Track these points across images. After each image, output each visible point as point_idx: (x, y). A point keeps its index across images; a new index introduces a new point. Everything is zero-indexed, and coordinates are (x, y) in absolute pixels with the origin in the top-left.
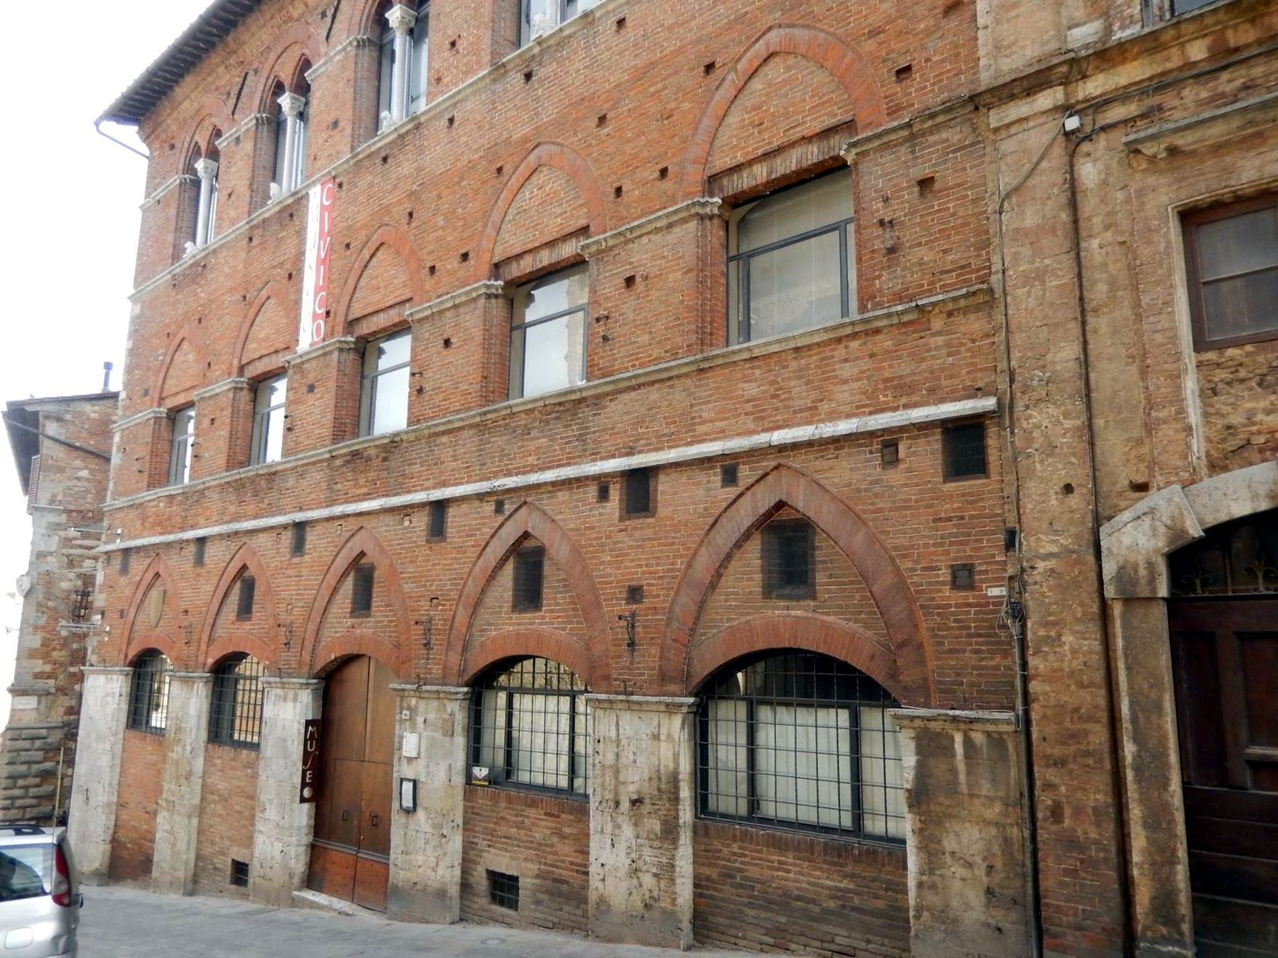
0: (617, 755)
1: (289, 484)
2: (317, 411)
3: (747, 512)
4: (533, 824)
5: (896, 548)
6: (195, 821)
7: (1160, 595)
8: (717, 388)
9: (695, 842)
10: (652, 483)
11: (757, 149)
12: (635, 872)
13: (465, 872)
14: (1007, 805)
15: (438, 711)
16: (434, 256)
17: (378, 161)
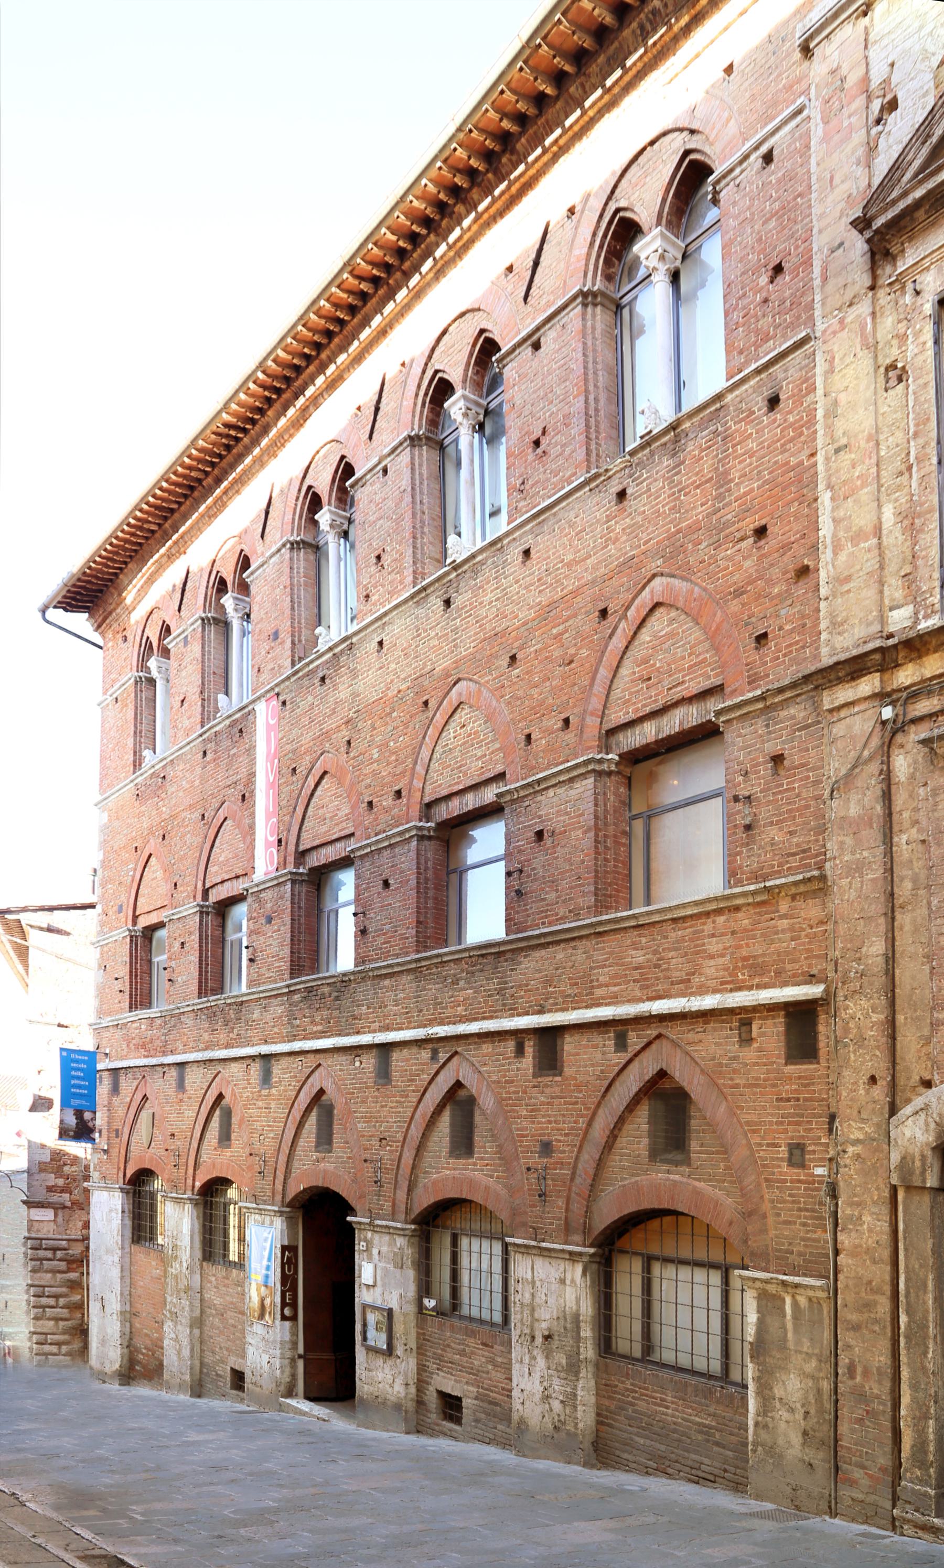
0: (533, 1295)
1: (255, 1016)
2: (275, 943)
3: (632, 1082)
4: (472, 1353)
5: (748, 1123)
6: (197, 1332)
7: (928, 1185)
8: (611, 953)
9: (597, 1376)
10: (559, 1043)
11: (644, 706)
12: (546, 1398)
13: (419, 1390)
14: (820, 1361)
15: (390, 1245)
16: (369, 791)
17: (317, 681)
